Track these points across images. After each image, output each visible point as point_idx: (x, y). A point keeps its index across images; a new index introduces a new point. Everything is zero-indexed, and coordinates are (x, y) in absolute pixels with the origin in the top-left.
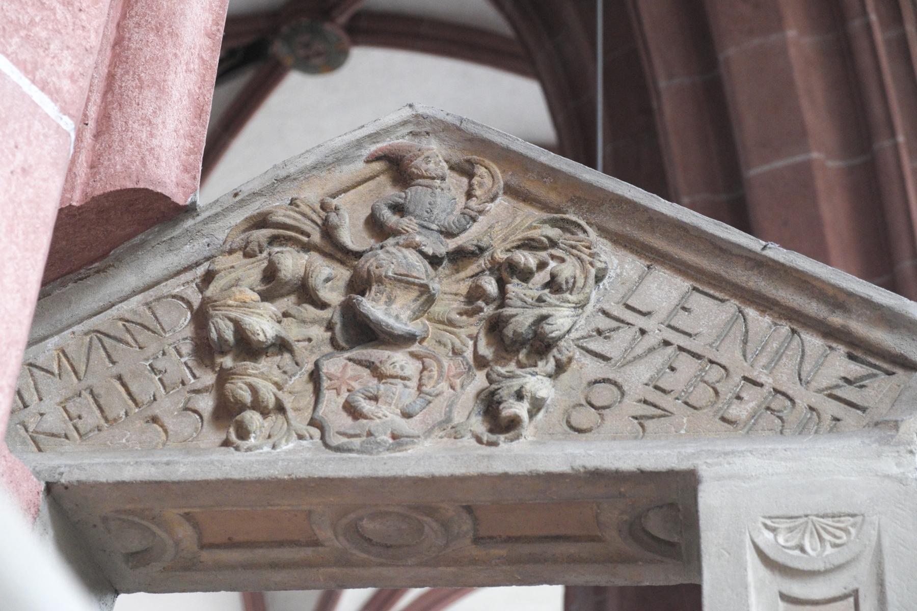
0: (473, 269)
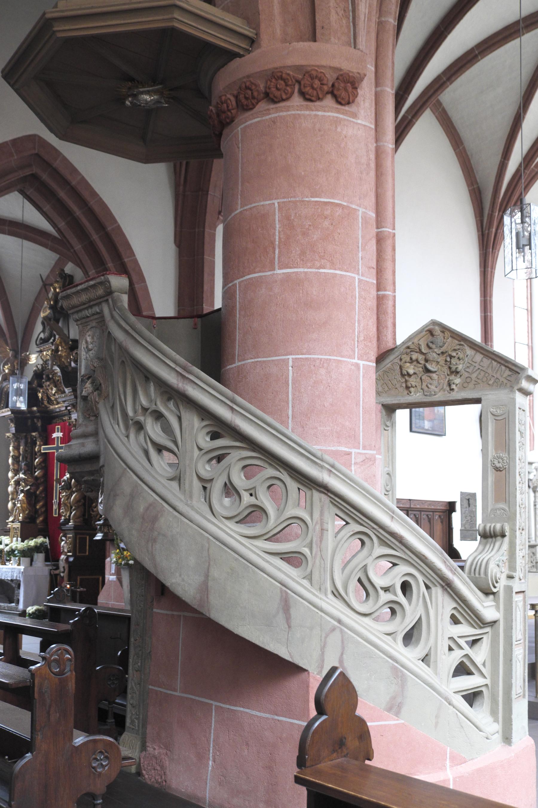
0: (445, 355)
